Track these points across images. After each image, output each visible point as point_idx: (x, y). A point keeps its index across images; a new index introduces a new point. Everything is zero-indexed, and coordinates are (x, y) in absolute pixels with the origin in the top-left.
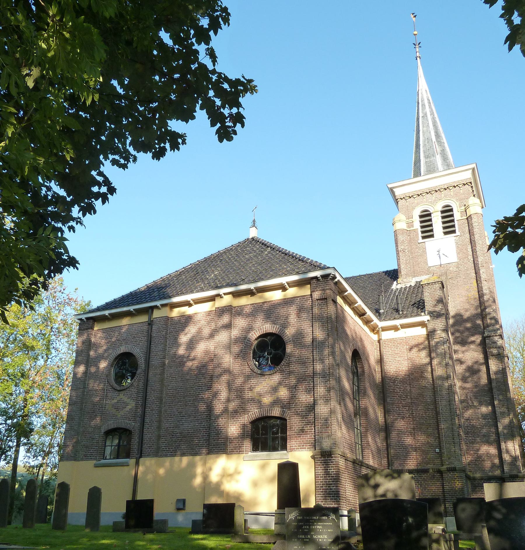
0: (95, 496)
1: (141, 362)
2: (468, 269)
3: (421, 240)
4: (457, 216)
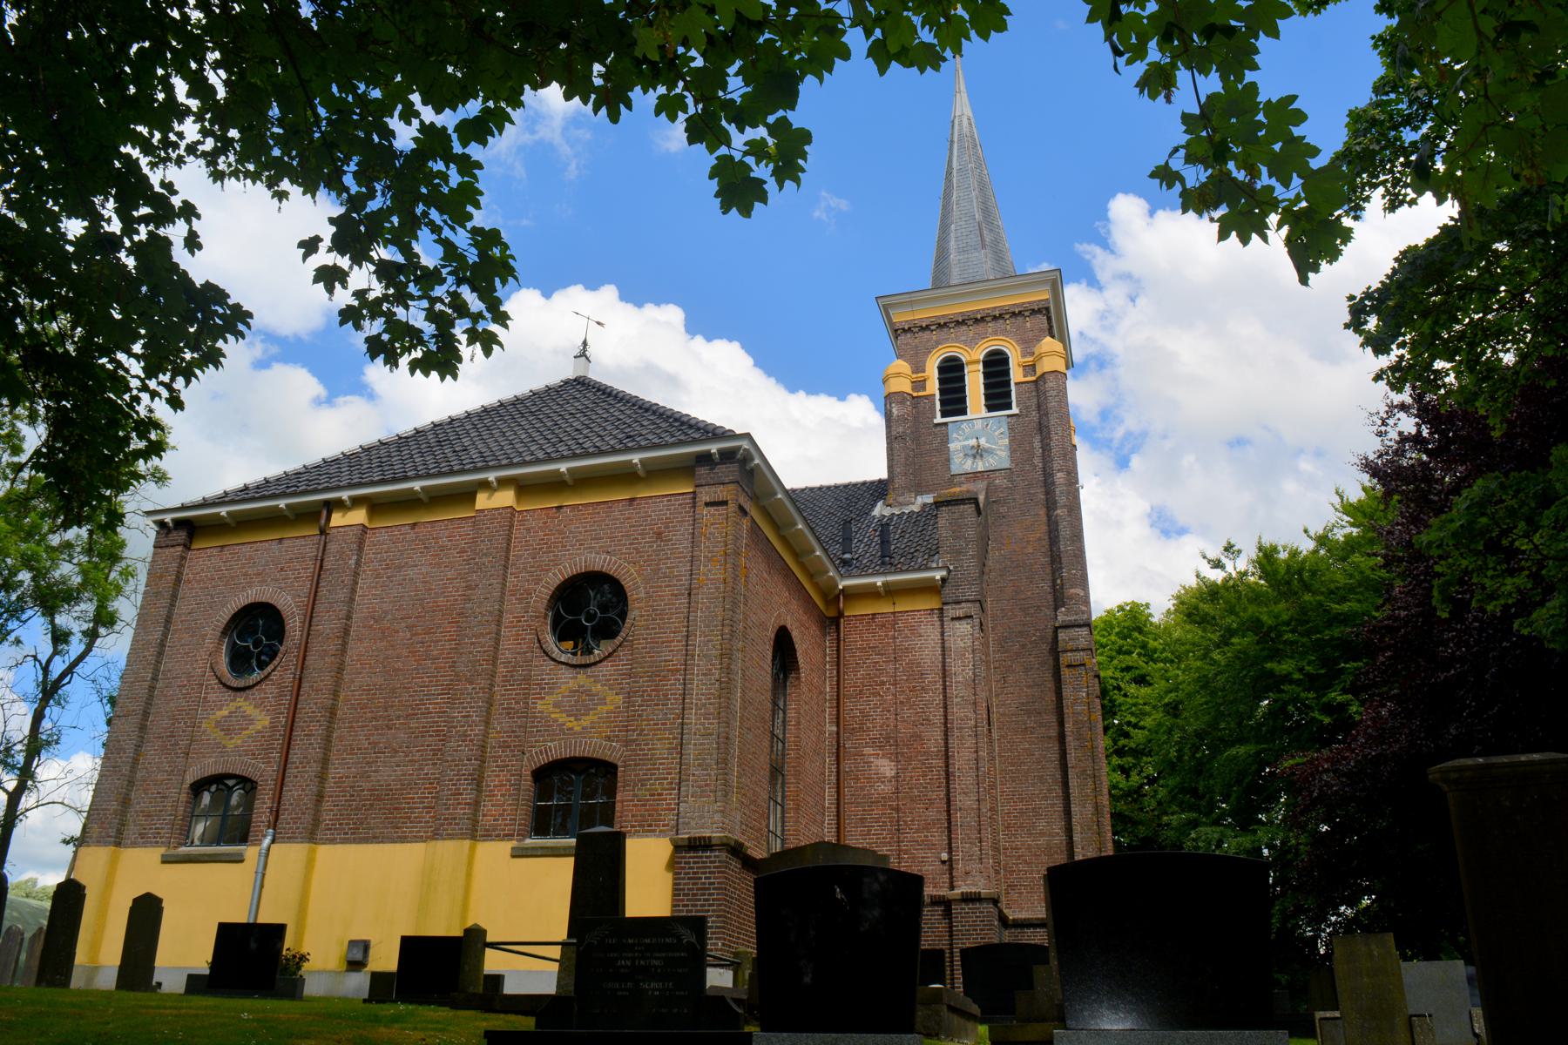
0: (146, 913)
1: (294, 626)
2: (1030, 485)
3: (939, 419)
4: (1016, 375)
